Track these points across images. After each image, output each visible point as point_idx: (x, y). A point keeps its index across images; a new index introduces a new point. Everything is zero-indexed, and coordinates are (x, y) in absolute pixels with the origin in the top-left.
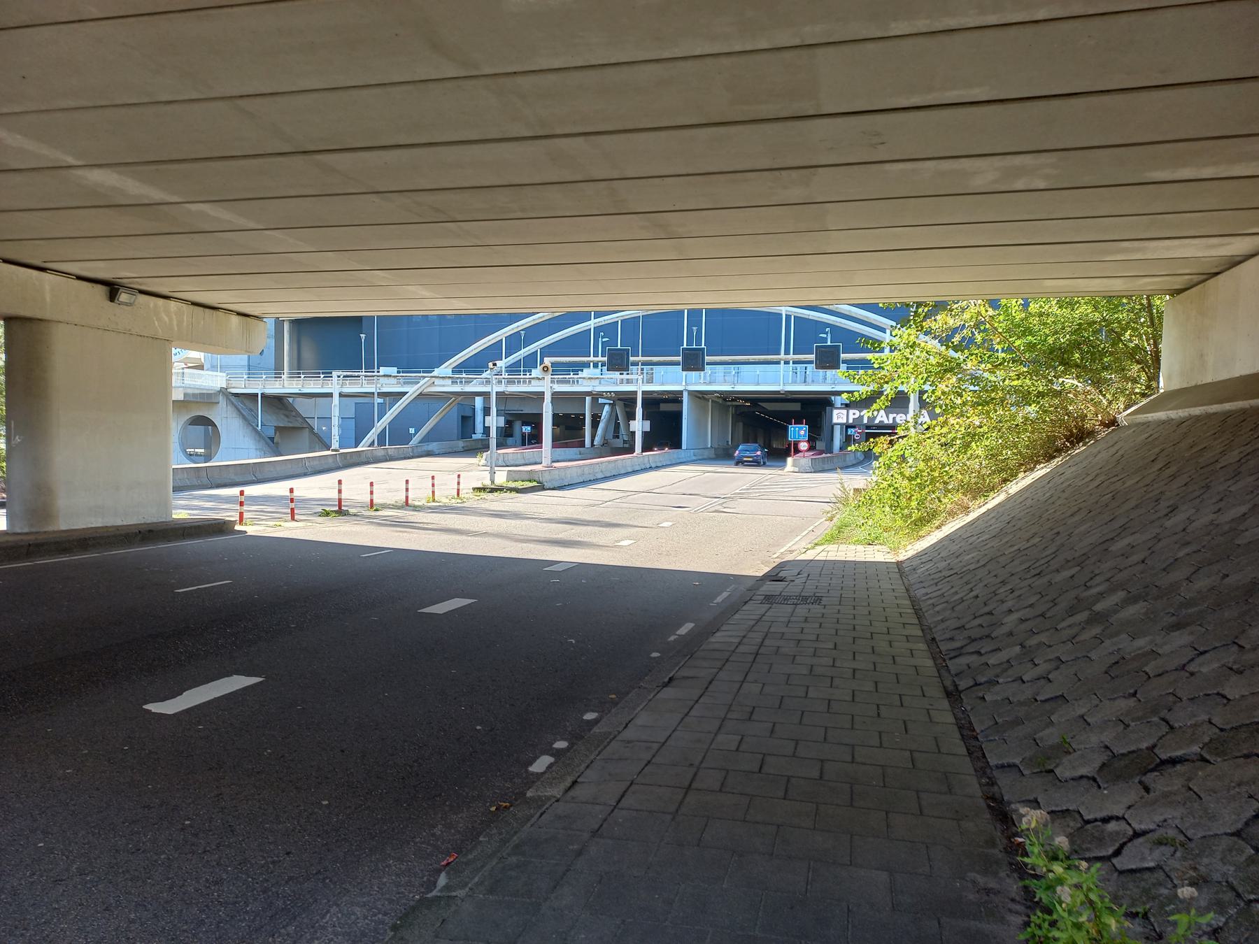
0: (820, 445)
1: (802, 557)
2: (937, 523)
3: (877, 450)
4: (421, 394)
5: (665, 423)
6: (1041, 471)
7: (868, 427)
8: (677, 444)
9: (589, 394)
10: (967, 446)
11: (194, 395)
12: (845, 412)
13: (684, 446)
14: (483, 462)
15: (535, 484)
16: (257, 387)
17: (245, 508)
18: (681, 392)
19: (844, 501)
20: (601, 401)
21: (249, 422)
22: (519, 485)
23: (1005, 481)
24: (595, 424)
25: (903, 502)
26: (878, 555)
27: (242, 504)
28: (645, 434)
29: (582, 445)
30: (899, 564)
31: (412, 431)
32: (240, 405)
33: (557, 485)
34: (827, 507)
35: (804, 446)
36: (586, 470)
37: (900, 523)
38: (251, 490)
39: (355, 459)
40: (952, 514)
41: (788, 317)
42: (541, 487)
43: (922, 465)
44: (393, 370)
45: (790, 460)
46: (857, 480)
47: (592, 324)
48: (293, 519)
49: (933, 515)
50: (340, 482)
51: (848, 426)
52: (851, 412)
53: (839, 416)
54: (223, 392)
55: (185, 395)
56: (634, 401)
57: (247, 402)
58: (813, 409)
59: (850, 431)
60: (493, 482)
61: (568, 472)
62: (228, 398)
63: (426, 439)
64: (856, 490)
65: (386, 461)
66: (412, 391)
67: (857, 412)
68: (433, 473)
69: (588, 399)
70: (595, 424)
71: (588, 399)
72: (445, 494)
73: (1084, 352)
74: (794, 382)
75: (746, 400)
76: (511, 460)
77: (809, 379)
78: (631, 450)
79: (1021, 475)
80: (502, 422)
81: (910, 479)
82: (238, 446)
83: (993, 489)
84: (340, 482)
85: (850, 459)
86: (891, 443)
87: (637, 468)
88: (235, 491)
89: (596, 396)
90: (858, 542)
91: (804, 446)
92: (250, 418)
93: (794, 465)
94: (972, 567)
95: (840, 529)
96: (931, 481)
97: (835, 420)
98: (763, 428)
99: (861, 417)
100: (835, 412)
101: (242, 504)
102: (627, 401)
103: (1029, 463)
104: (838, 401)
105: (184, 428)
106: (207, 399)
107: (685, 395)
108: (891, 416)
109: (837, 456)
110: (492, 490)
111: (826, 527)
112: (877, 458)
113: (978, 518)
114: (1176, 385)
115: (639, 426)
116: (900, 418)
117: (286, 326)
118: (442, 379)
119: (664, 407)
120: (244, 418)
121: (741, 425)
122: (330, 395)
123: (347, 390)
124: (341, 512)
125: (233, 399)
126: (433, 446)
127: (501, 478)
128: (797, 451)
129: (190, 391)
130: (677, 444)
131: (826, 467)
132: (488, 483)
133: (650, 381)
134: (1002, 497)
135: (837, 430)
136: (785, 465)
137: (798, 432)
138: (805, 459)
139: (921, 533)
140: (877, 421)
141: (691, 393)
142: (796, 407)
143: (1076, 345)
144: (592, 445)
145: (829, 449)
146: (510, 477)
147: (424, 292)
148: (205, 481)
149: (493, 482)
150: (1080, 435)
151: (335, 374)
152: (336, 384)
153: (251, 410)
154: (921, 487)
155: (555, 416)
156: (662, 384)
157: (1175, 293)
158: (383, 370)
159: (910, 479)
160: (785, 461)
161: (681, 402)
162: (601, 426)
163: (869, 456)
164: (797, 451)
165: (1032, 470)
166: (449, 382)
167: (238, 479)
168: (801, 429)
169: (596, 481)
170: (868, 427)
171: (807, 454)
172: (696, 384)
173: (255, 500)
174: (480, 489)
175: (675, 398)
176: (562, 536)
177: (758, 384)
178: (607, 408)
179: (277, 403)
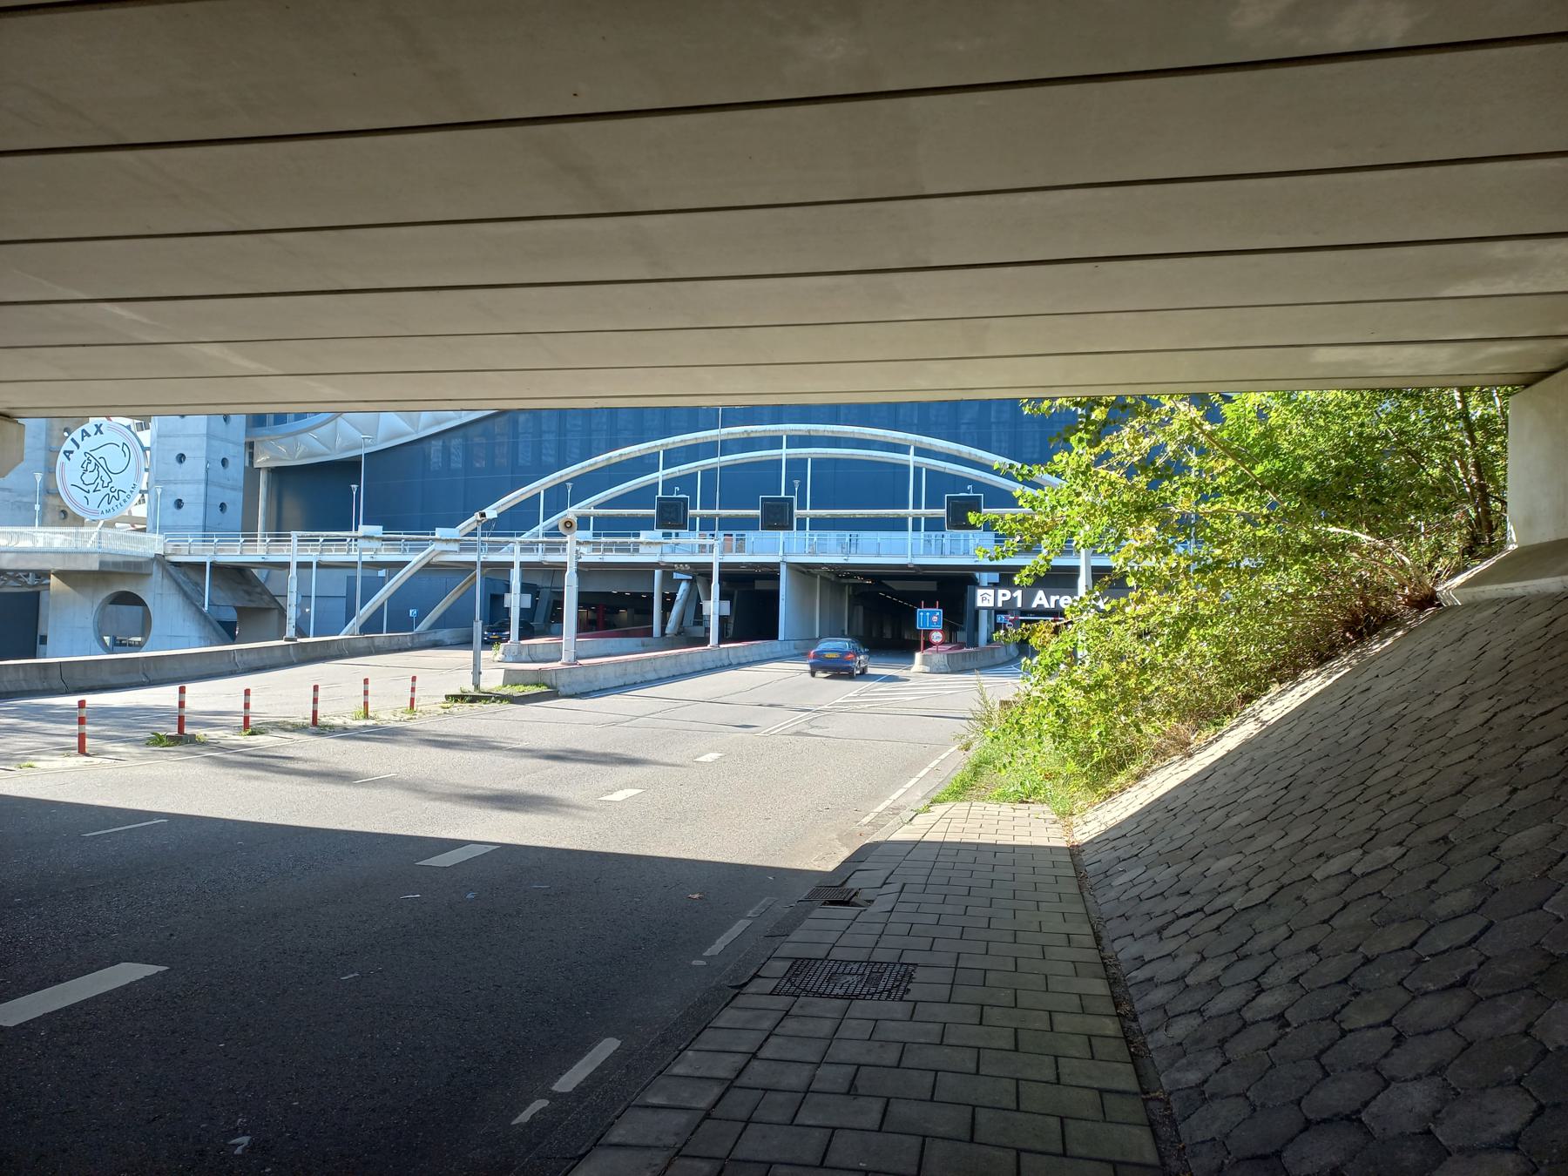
0: (962, 636)
1: (901, 835)
2: (1135, 769)
3: (1033, 641)
4: (428, 565)
5: (753, 607)
6: (1313, 684)
7: (1023, 613)
8: (772, 634)
9: (656, 565)
10: (1180, 637)
11: (115, 564)
12: (991, 592)
13: (781, 637)
14: (499, 656)
15: (544, 689)
16: (205, 554)
17: (88, 729)
18: (777, 565)
19: (986, 721)
20: (676, 576)
21: (191, 599)
22: (517, 691)
23: (1248, 698)
24: (668, 605)
25: (1076, 730)
26: (1035, 828)
27: (82, 721)
28: (722, 619)
29: (649, 633)
30: (1074, 852)
31: (413, 613)
32: (181, 578)
33: (579, 689)
34: (960, 727)
35: (937, 637)
36: (631, 669)
37: (1072, 766)
38: (92, 700)
39: (333, 650)
40: (1160, 753)
41: (918, 470)
42: (554, 694)
43: (1106, 668)
44: (377, 530)
45: (918, 656)
46: (1003, 687)
47: (660, 475)
48: (82, 750)
49: (1131, 753)
50: (247, 692)
51: (998, 611)
52: (1001, 592)
53: (985, 598)
54: (160, 560)
55: (102, 563)
56: (709, 576)
57: (192, 574)
58: (951, 589)
59: (1001, 618)
60: (477, 687)
61: (601, 671)
62: (164, 568)
63: (436, 625)
64: (1004, 703)
65: (370, 654)
66: (416, 559)
67: (1007, 592)
68: (414, 672)
69: (658, 573)
70: (668, 605)
71: (658, 573)
72: (387, 712)
73: (1357, 486)
74: (927, 553)
75: (866, 577)
76: (540, 653)
77: (947, 550)
78: (705, 641)
79: (1275, 688)
80: (527, 601)
81: (1087, 690)
82: (175, 632)
83: (1229, 712)
84: (247, 692)
85: (1000, 655)
86: (1056, 631)
87: (711, 665)
88: (72, 701)
89: (669, 570)
90: (1004, 797)
91: (937, 637)
92: (195, 596)
93: (924, 662)
94: (1239, 900)
95: (977, 770)
96: (1121, 693)
97: (979, 603)
98: (884, 616)
99: (1013, 600)
100: (980, 592)
101: (82, 721)
102: (700, 573)
103: (1286, 670)
104: (984, 578)
105: (102, 608)
106: (135, 569)
107: (783, 569)
108: (1053, 599)
109: (983, 650)
110: (474, 699)
111: (953, 762)
112: (1035, 653)
113: (1212, 769)
114: (1545, 533)
115: (714, 607)
116: (1065, 601)
117: (263, 477)
118: (446, 544)
119: (760, 585)
120: (186, 595)
121: (861, 608)
122: (286, 565)
123: (329, 557)
124: (181, 739)
125: (172, 569)
126: (444, 634)
127: (493, 680)
128: (929, 644)
129: (109, 558)
130: (772, 634)
131: (968, 665)
132: (469, 688)
133: (740, 549)
134: (1249, 729)
135: (983, 616)
136: (912, 662)
137: (930, 618)
138: (938, 656)
139: (1111, 786)
140: (1034, 605)
141: (791, 566)
142: (931, 586)
143: (1347, 475)
144: (663, 633)
145: (973, 641)
146: (511, 678)
147: (238, 360)
148: (57, 683)
149: (477, 687)
150: (1366, 622)
151: (294, 534)
152: (294, 550)
153: (197, 584)
154: (1105, 707)
155: (581, 595)
156: (753, 554)
157: (1531, 380)
158: (364, 529)
159: (1087, 690)
160: (913, 657)
161: (777, 578)
162: (676, 609)
163: (1024, 648)
164: (929, 644)
165: (1294, 677)
166: (455, 547)
167: (113, 681)
168: (933, 614)
169: (635, 685)
170: (1023, 613)
171: (941, 648)
172: (797, 554)
173: (105, 713)
174: (459, 698)
175: (770, 573)
176: (508, 786)
177: (879, 555)
178: (684, 586)
179: (235, 575)
